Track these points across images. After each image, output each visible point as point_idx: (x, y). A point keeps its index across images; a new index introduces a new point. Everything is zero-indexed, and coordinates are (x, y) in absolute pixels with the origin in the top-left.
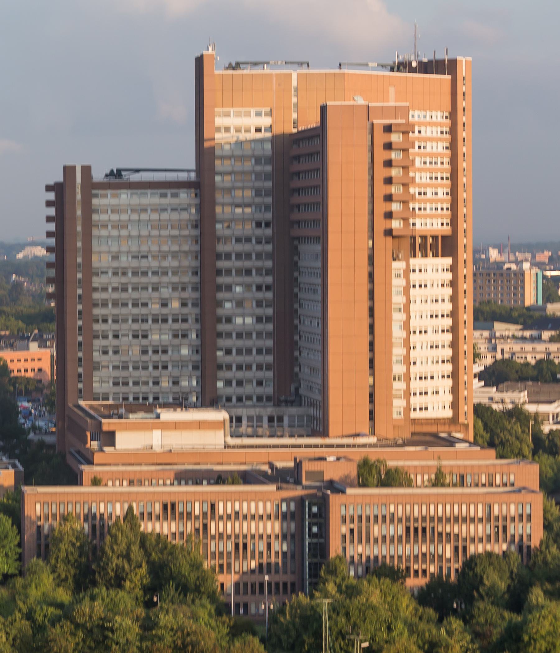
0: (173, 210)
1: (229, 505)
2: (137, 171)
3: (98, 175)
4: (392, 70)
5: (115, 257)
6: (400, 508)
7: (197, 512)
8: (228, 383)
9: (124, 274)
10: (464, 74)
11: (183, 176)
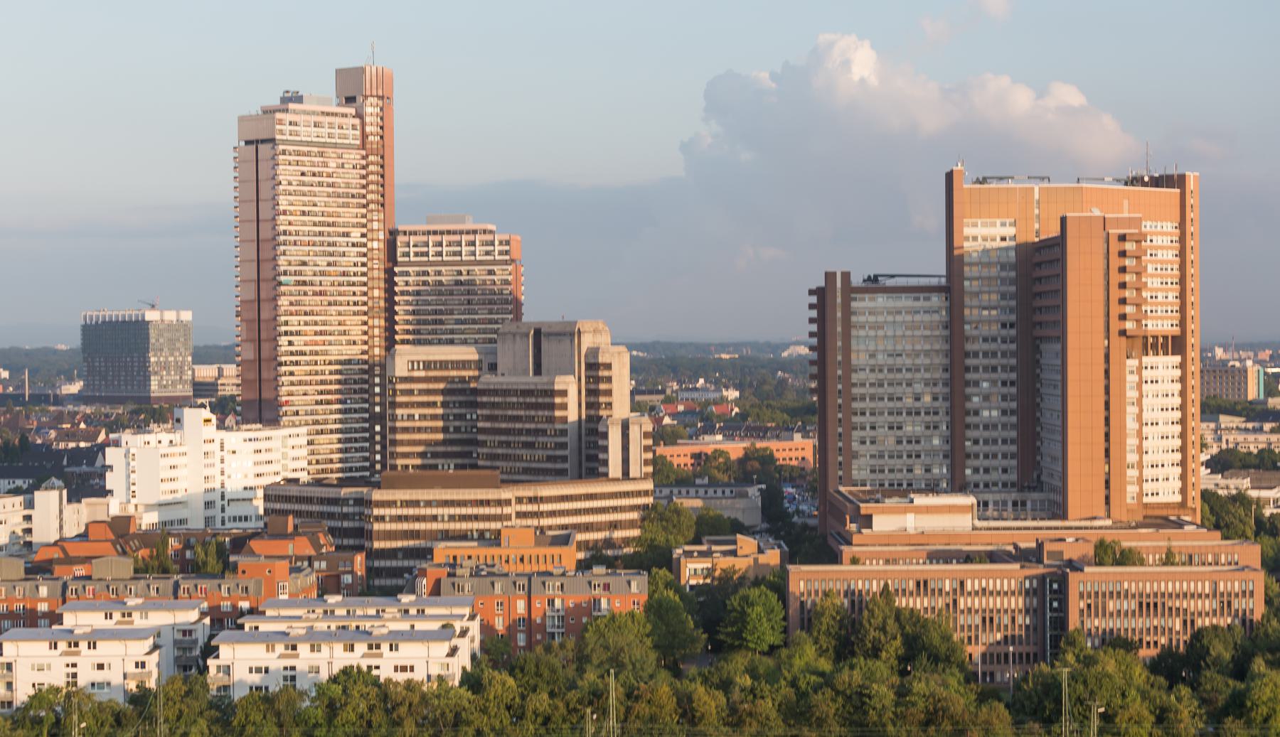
1: (976, 582)
2: (893, 276)
3: (857, 280)
4: (1126, 184)
5: (872, 356)
7: (947, 589)
8: (976, 470)
9: (881, 371)
11: (934, 282)
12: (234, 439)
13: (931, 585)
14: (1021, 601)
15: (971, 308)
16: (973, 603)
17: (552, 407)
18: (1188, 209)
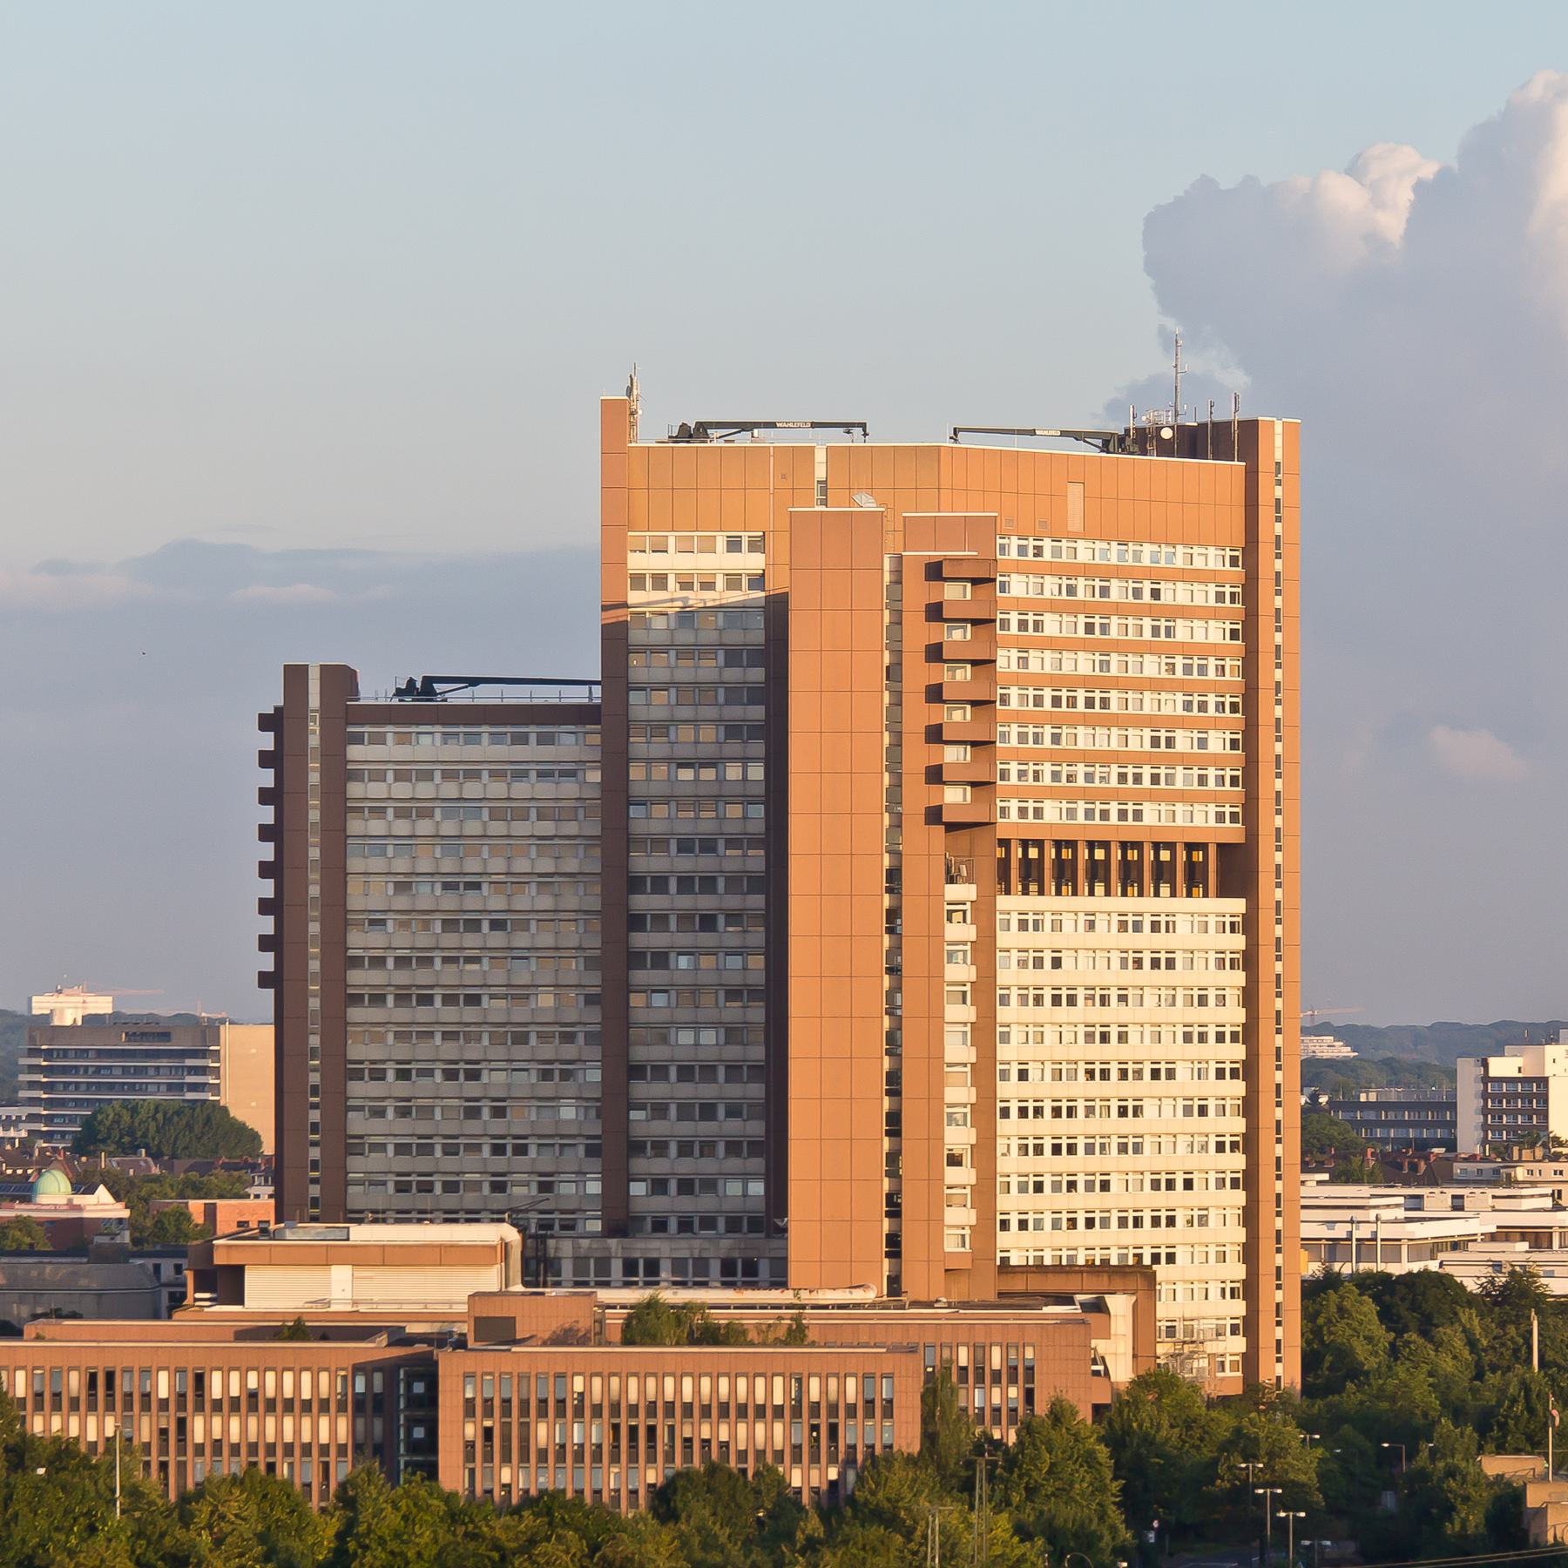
0: (542, 774)
1: (235, 1377)
2: (474, 682)
3: (375, 689)
4: (1105, 448)
5: (402, 887)
6: (597, 1382)
7: (163, 1392)
8: (659, 1186)
10: (1278, 456)
11: (577, 695)
13: (122, 1385)
14: (343, 1425)
15: (649, 761)
16: (226, 1429)
18: (1265, 512)
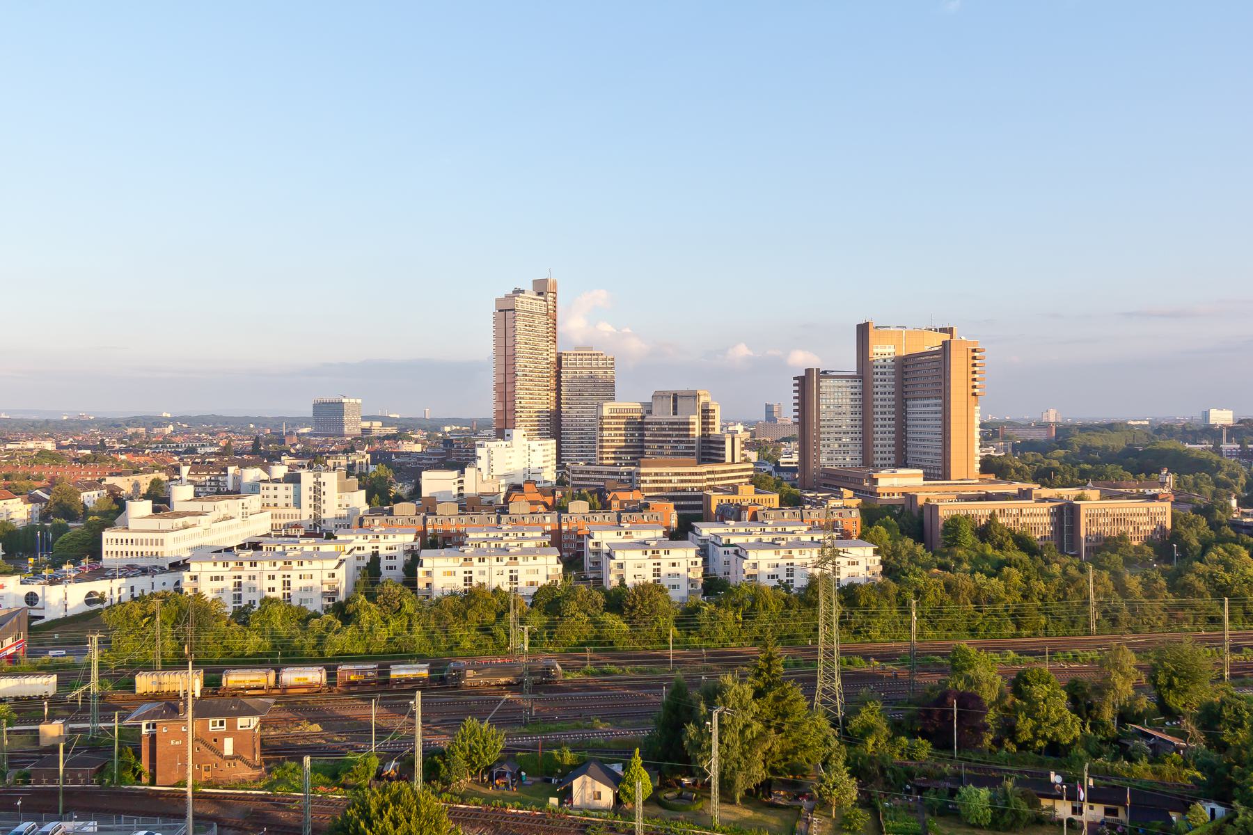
12: (534, 444)
17: (688, 430)
